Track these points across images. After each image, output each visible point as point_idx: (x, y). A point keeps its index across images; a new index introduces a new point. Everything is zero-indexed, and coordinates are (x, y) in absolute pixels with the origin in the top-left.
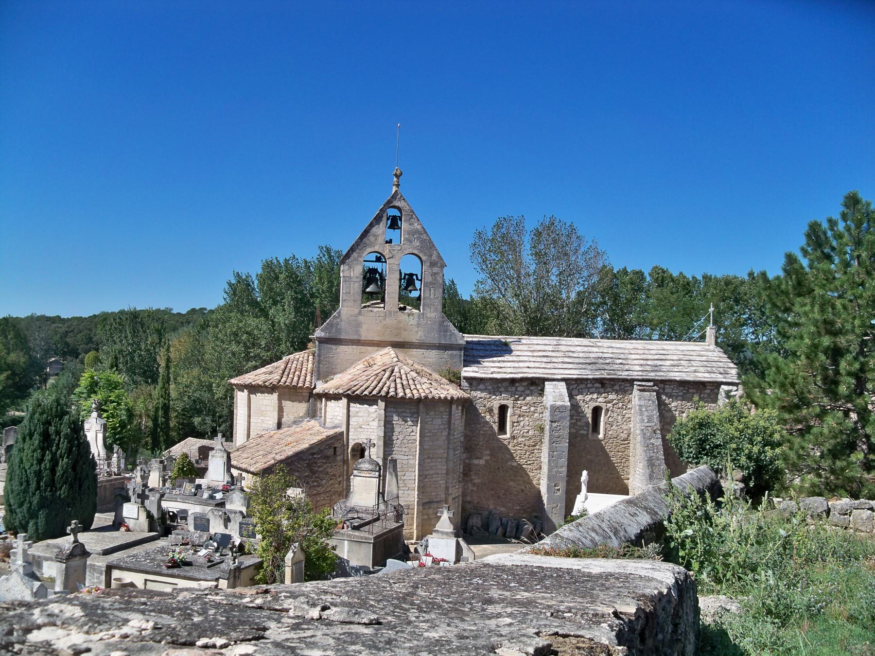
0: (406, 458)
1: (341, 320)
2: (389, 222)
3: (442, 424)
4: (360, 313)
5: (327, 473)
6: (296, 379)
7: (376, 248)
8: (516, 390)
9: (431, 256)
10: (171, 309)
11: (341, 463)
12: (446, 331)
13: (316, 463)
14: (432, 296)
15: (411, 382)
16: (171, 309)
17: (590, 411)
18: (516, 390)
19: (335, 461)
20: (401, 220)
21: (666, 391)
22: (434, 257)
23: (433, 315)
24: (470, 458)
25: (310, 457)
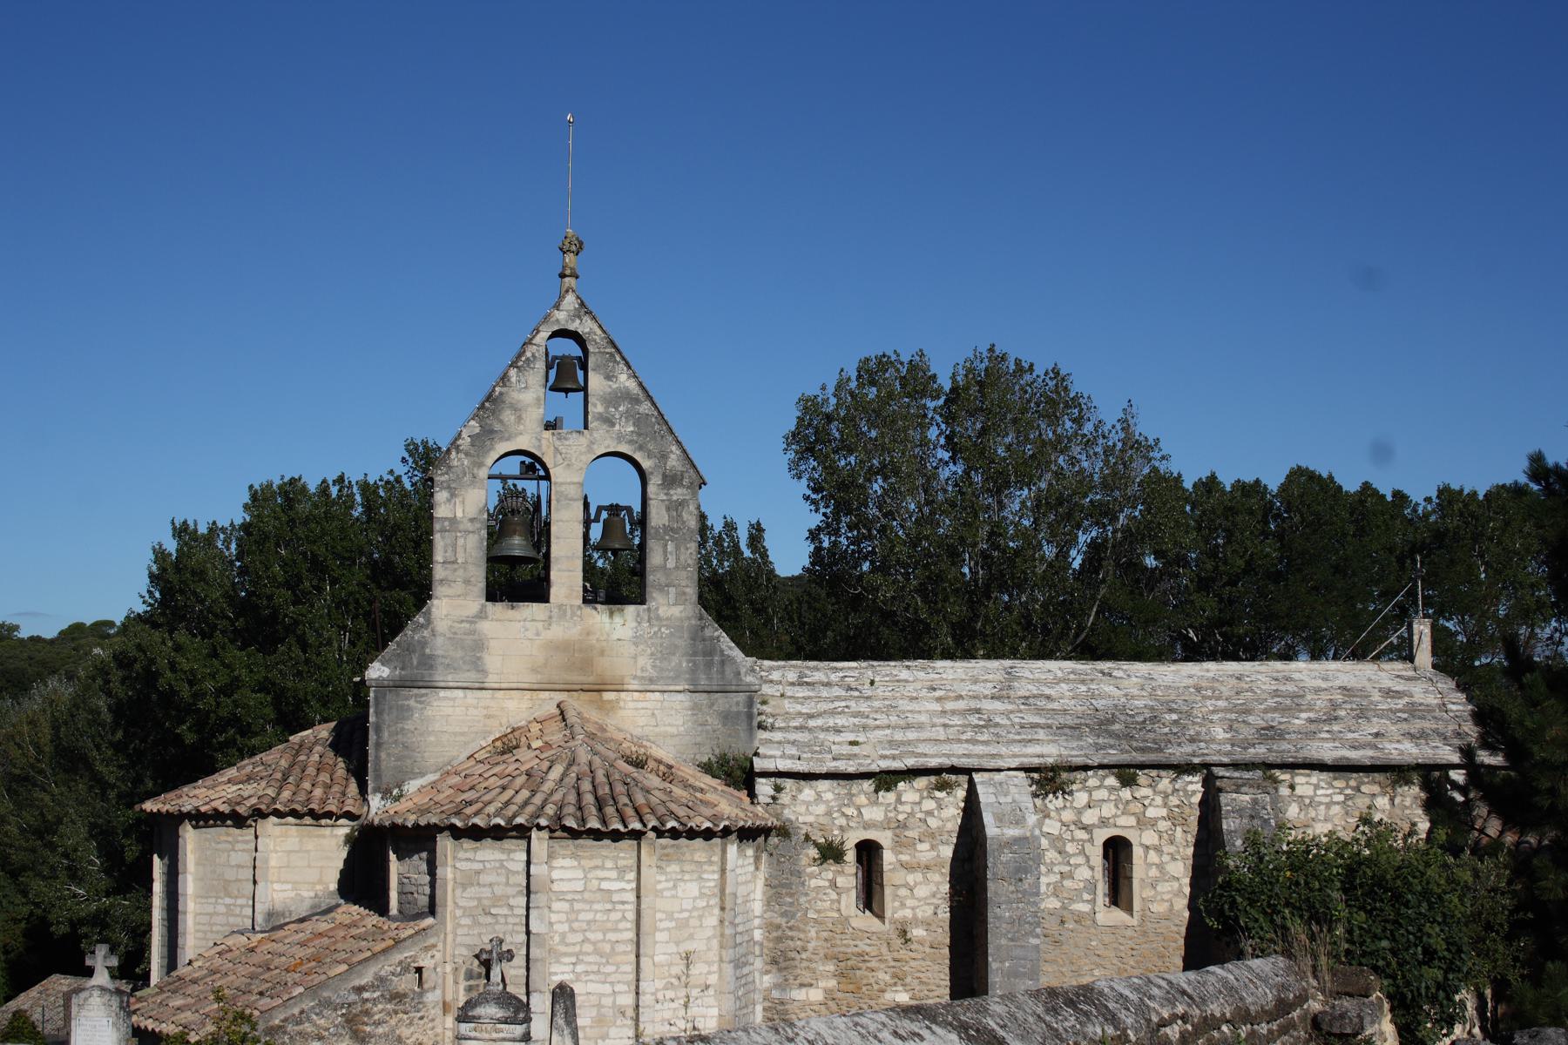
0: (607, 989)
1: (434, 634)
2: (553, 373)
3: (702, 895)
4: (482, 615)
6: (318, 792)
7: (523, 443)
8: (899, 801)
9: (664, 457)
10: (17, 628)
13: (367, 1013)
14: (671, 564)
15: (619, 788)
16: (17, 628)
17: (1099, 851)
18: (899, 801)
19: (418, 1003)
20: (585, 367)
21: (1299, 791)
22: (674, 461)
24: (782, 986)
25: (353, 997)
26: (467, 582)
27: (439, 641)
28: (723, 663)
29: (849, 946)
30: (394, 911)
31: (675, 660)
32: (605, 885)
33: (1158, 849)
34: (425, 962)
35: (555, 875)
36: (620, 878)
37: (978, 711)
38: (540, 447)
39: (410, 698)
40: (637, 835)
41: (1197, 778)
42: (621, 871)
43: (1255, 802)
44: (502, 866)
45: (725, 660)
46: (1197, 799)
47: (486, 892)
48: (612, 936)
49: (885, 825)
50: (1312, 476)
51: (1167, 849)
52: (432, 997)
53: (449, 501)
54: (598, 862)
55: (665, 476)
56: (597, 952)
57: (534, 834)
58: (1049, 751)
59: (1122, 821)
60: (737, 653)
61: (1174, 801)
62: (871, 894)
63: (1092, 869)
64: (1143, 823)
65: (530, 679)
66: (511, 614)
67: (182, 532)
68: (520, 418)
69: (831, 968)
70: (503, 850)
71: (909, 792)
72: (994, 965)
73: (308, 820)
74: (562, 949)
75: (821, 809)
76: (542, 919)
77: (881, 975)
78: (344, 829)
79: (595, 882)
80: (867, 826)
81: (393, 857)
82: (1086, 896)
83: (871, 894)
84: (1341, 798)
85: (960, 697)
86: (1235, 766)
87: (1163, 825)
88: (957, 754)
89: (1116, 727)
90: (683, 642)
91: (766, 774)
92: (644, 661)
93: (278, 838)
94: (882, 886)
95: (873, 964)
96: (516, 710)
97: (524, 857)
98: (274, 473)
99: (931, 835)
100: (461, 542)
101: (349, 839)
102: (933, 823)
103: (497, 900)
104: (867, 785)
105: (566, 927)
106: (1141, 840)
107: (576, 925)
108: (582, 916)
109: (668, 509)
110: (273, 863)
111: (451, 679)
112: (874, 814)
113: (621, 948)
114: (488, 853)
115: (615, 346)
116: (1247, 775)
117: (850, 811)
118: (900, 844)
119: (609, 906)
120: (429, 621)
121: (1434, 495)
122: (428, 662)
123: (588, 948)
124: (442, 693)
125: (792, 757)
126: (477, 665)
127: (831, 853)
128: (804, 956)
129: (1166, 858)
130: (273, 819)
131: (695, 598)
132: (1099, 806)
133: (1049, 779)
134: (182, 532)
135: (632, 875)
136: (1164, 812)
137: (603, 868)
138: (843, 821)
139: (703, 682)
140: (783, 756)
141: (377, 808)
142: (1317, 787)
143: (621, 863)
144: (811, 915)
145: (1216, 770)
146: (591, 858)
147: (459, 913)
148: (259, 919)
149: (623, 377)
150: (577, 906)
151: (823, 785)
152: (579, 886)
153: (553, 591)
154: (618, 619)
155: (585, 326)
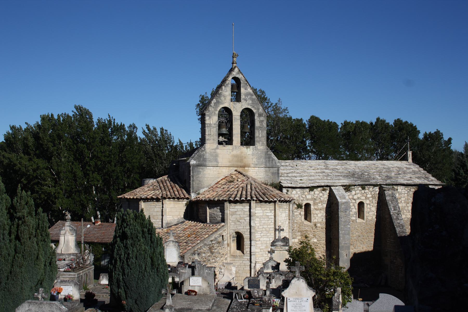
4: (217, 148)
5: (220, 253)
8: (314, 194)
9: (258, 109)
11: (226, 246)
13: (213, 247)
14: (260, 136)
18: (314, 194)
21: (399, 191)
25: (210, 243)
26: (214, 140)
27: (207, 154)
28: (272, 160)
29: (303, 228)
30: (208, 222)
31: (262, 159)
32: (267, 214)
33: (369, 204)
34: (224, 234)
35: (256, 212)
36: (271, 212)
37: (324, 172)
39: (200, 169)
40: (275, 202)
41: (378, 188)
42: (271, 211)
43: (392, 193)
44: (242, 210)
45: (273, 160)
46: (378, 193)
47: (238, 216)
48: (269, 227)
49: (311, 199)
50: (317, 118)
51: (372, 204)
52: (226, 242)
54: (266, 208)
55: (259, 114)
56: (266, 230)
57: (252, 202)
58: (346, 182)
59: (362, 198)
60: (275, 158)
61: (373, 193)
62: (307, 216)
63: (355, 210)
64: (367, 198)
65: (228, 164)
66: (224, 148)
67: (13, 128)
68: (225, 99)
69: (300, 234)
70: (243, 206)
71: (317, 191)
72: (340, 232)
73: (176, 200)
74: (258, 230)
75: (297, 196)
76: (254, 222)
77: (311, 235)
78: (185, 202)
80: (307, 200)
81: (208, 208)
82: (355, 216)
83: (307, 216)
84: (406, 192)
85: (318, 169)
86: (386, 185)
87: (371, 199)
88: (329, 182)
89: (356, 176)
90: (263, 155)
91: (285, 187)
92: (254, 160)
93: (168, 204)
94: (311, 214)
95: (309, 233)
96: (226, 172)
97: (248, 207)
98: (46, 112)
99: (321, 202)
100: (212, 130)
101: (186, 204)
102: (322, 199)
103: (241, 218)
104: (308, 190)
105: (259, 225)
106: (366, 202)
108: (262, 222)
110: (167, 211)
111: (210, 164)
112: (309, 197)
113: (271, 229)
114: (239, 207)
115: (247, 81)
116: (390, 187)
117: (304, 196)
118: (315, 204)
120: (205, 150)
121: (343, 123)
122: (205, 160)
123: (264, 229)
124: (208, 168)
125: (289, 183)
126: (216, 161)
127: (299, 206)
129: (371, 206)
130: (167, 200)
131: (266, 144)
132: (357, 194)
133: (347, 188)
134: (13, 128)
135: (273, 212)
136: (371, 196)
137: (267, 210)
138: (302, 199)
139: (268, 165)
140: (287, 183)
141: (193, 196)
142: (402, 190)
143: (271, 209)
144: (295, 221)
145: (383, 186)
146: (264, 207)
147: (231, 222)
148: (164, 225)
149: (249, 89)
150: (261, 219)
151: (298, 190)
152: (262, 214)
153: (234, 142)
154: (248, 149)
155: (240, 76)
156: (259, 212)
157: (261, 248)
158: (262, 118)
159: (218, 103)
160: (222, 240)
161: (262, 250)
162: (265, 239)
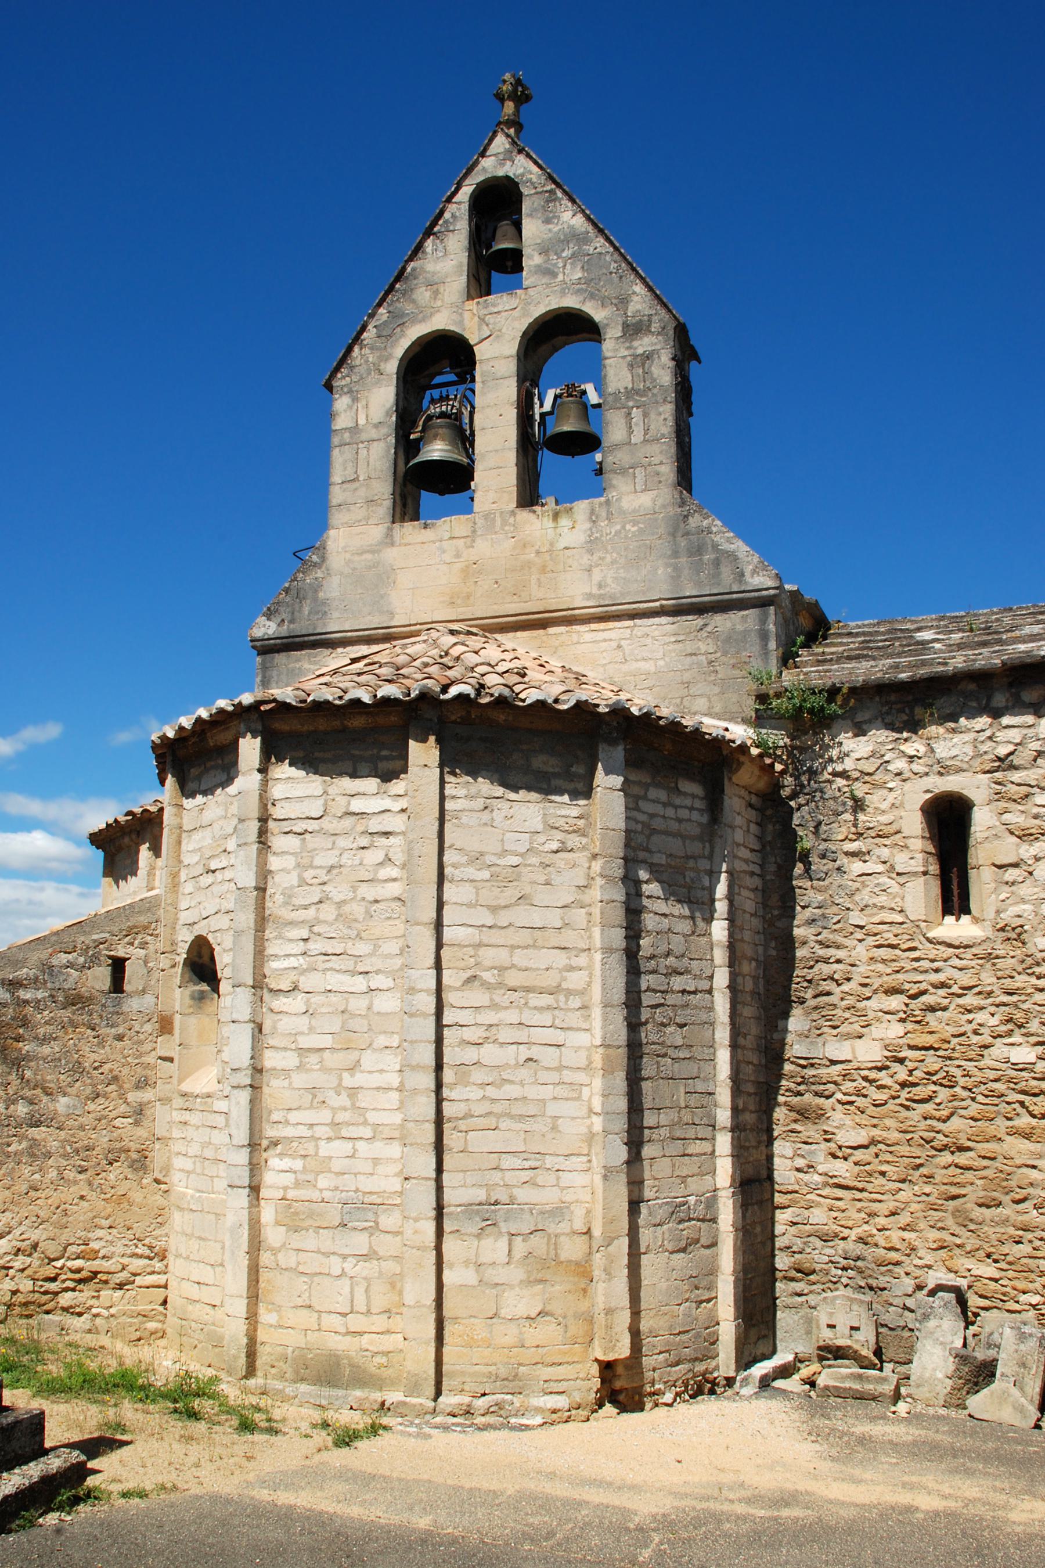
0: (360, 983)
4: (389, 540)
5: (78, 1069)
9: (623, 302)
12: (697, 550)
13: (25, 1023)
14: (637, 437)
23: (645, 500)
32: (356, 805)
38: (461, 323)
48: (368, 892)
53: (350, 407)
55: (626, 326)
66: (428, 534)
79: (342, 801)
100: (363, 453)
107: (308, 875)
109: (631, 366)
119: (364, 841)
120: (323, 559)
128: (846, 987)
154: (564, 522)
156: (299, 791)
157: (305, 1042)
158: (644, 344)
159: (399, 320)
160: (106, 983)
161: (313, 1059)
162: (335, 981)
